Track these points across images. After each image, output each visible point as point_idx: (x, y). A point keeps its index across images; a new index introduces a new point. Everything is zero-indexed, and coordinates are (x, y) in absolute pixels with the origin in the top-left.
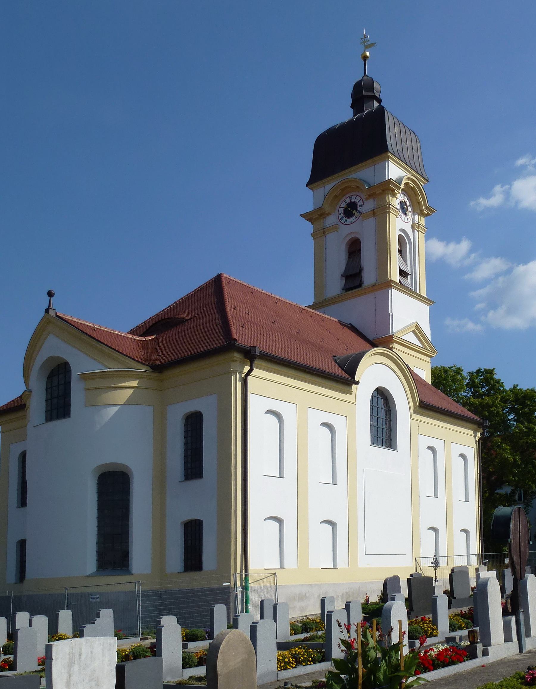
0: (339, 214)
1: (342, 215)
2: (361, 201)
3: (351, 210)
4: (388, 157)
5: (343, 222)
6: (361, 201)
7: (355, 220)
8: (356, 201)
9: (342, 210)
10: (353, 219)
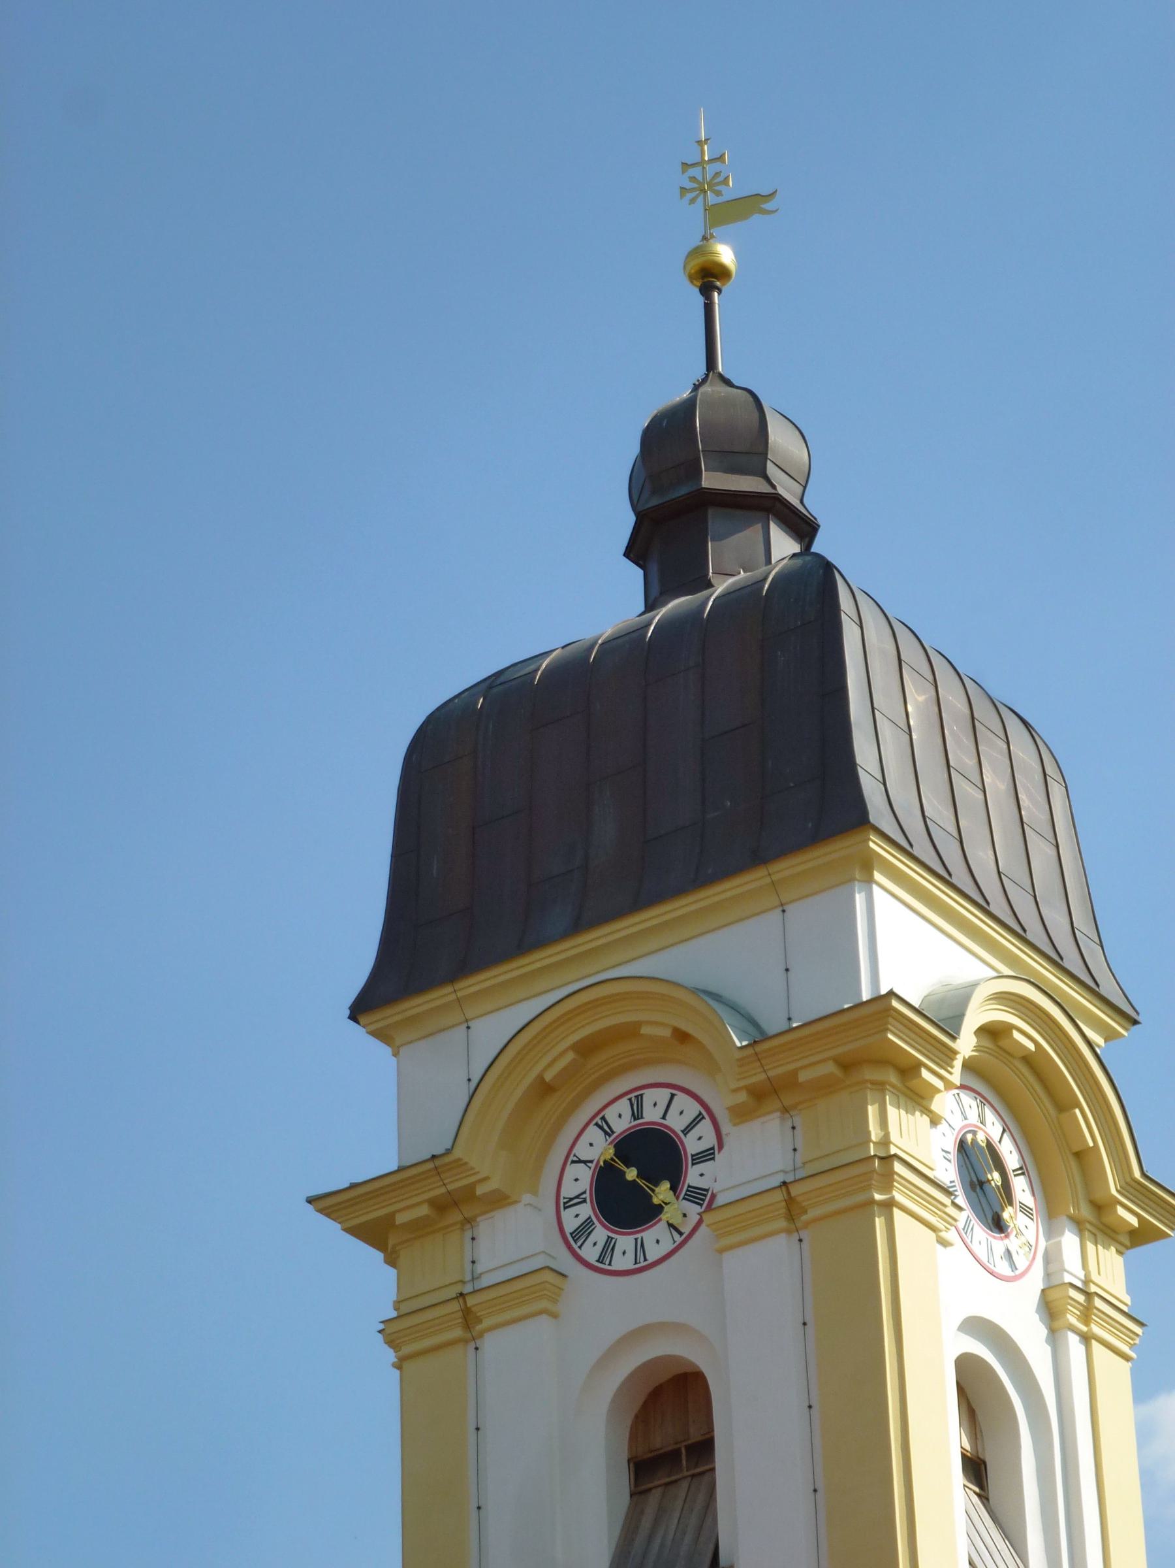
0: (563, 1204)
1: (586, 1210)
2: (706, 1127)
3: (638, 1180)
4: (867, 865)
5: (590, 1253)
6: (706, 1127)
7: (667, 1246)
8: (676, 1123)
9: (580, 1180)
10: (656, 1239)
